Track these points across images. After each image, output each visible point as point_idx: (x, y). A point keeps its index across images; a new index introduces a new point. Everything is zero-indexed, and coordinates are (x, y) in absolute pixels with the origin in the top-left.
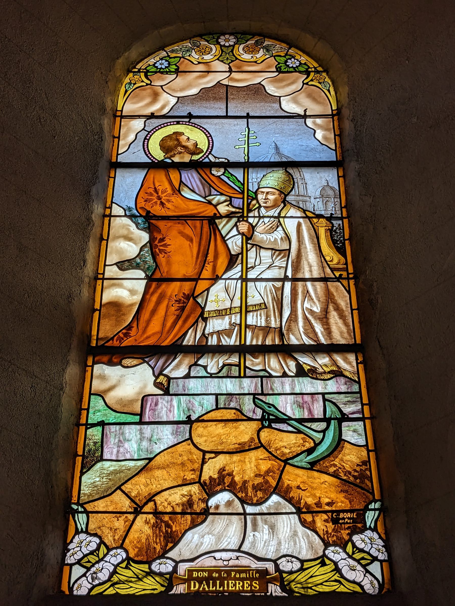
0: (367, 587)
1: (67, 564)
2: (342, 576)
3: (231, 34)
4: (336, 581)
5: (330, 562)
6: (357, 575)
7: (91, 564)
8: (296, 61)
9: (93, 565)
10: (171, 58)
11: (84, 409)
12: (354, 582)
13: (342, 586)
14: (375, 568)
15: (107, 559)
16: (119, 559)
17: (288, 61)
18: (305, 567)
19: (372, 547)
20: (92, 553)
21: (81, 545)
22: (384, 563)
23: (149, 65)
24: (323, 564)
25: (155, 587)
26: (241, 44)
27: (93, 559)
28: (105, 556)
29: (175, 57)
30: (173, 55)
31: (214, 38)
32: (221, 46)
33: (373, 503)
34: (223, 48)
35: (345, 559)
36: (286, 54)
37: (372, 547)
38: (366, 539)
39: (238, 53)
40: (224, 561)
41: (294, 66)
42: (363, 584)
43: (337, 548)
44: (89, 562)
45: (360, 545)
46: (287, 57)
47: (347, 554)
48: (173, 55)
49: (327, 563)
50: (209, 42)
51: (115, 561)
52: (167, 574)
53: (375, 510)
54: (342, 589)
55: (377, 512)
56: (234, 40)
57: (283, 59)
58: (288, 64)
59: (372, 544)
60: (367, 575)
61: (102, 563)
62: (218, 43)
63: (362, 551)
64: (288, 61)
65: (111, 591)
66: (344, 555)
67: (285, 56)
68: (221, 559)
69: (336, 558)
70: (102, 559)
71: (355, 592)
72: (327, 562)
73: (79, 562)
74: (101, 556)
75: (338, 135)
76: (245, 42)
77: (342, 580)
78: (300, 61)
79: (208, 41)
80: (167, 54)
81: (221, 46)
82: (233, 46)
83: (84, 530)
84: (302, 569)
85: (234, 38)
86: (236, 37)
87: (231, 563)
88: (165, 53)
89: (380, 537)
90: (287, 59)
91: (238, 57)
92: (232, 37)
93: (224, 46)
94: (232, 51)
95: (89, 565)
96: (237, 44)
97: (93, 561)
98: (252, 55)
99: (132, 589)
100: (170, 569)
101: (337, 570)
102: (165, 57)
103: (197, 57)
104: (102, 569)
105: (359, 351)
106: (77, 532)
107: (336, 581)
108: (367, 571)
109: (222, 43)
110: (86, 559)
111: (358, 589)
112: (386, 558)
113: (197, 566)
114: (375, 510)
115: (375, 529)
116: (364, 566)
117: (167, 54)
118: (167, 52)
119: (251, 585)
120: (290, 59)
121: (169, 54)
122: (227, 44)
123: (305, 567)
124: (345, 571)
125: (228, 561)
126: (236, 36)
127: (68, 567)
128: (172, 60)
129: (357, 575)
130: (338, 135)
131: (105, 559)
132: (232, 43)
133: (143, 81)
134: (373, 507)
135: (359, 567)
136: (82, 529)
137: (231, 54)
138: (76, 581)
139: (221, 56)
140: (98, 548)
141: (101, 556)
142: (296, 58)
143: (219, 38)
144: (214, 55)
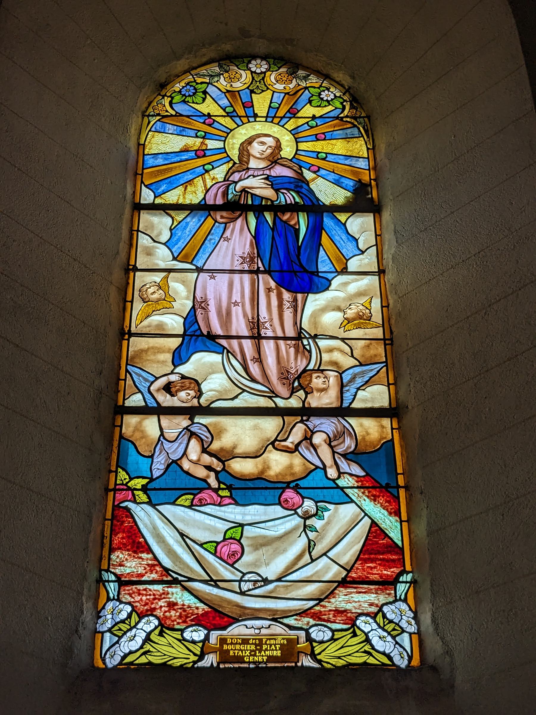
0: (397, 660)
1: (99, 632)
2: (373, 648)
3: (263, 58)
4: (365, 652)
5: (361, 632)
6: (387, 646)
7: (123, 632)
8: (330, 93)
9: (125, 633)
10: (197, 84)
11: (113, 472)
12: (384, 653)
13: (371, 657)
14: (405, 640)
15: (140, 626)
16: (152, 626)
17: (322, 93)
18: (335, 637)
19: (402, 619)
20: (123, 621)
21: (116, 612)
22: (413, 635)
23: (175, 92)
24: (355, 635)
25: (188, 656)
26: (273, 71)
27: (124, 627)
28: (137, 624)
29: (202, 83)
30: (199, 80)
31: (244, 62)
32: (252, 72)
33: (405, 575)
34: (253, 74)
35: (375, 630)
36: (321, 86)
37: (402, 619)
38: (397, 610)
39: (269, 82)
40: (255, 629)
41: (329, 99)
42: (392, 655)
43: (368, 618)
44: (120, 629)
45: (390, 616)
46: (322, 89)
47: (378, 625)
48: (199, 80)
49: (358, 634)
50: (239, 67)
51: (148, 628)
52: (199, 642)
53: (406, 582)
54: (371, 660)
55: (408, 585)
56: (266, 66)
57: (317, 90)
58: (321, 96)
59: (401, 616)
60: (397, 646)
61: (134, 630)
62: (249, 69)
63: (391, 621)
64: (322, 93)
65: (143, 660)
66: (375, 626)
67: (319, 88)
68: (253, 627)
69: (367, 628)
70: (135, 627)
71: (383, 664)
72: (358, 632)
73: (110, 630)
74: (133, 624)
75: (373, 180)
76: (277, 69)
77: (371, 651)
78: (335, 94)
79: (237, 66)
80: (194, 78)
81: (252, 72)
82: (265, 73)
83: (116, 597)
84: (333, 639)
85: (266, 64)
86: (269, 63)
87: (264, 631)
88: (191, 77)
89: (410, 609)
90: (321, 91)
91: (270, 87)
92: (264, 62)
93: (255, 72)
94: (263, 79)
95: (120, 633)
96: (269, 70)
97: (125, 630)
98: (284, 85)
99: (166, 657)
100: (202, 637)
101: (368, 640)
102: (192, 82)
103: (225, 83)
104: (135, 636)
105: (394, 417)
106: (109, 599)
107: (365, 652)
108: (397, 643)
109: (253, 69)
110: (116, 628)
111: (386, 661)
112: (416, 631)
113: (229, 634)
114: (406, 582)
115: (405, 601)
116: (394, 637)
117: (194, 78)
118: (193, 76)
119: (254, 659)
120: (324, 91)
121: (196, 79)
122: (258, 71)
123: (335, 637)
124: (375, 641)
125: (260, 629)
126: (267, 61)
127: (100, 635)
128: (199, 86)
129: (387, 646)
130: (373, 179)
131: (137, 627)
132: (264, 70)
133: (168, 112)
134: (405, 580)
135: (389, 638)
136: (114, 597)
137: (262, 81)
138: (108, 650)
139: (251, 83)
140: (129, 616)
141: (133, 624)
142: (330, 90)
143: (250, 62)
144: (244, 82)
